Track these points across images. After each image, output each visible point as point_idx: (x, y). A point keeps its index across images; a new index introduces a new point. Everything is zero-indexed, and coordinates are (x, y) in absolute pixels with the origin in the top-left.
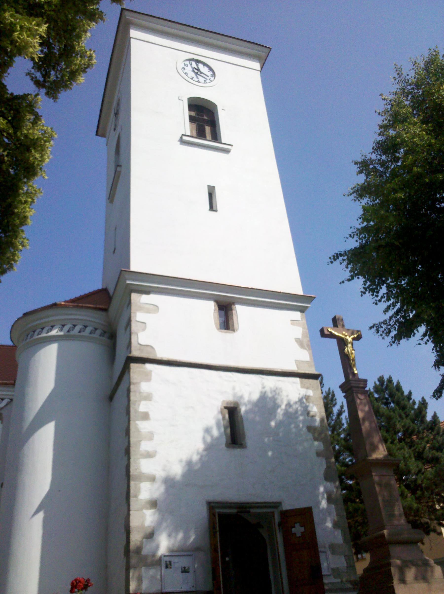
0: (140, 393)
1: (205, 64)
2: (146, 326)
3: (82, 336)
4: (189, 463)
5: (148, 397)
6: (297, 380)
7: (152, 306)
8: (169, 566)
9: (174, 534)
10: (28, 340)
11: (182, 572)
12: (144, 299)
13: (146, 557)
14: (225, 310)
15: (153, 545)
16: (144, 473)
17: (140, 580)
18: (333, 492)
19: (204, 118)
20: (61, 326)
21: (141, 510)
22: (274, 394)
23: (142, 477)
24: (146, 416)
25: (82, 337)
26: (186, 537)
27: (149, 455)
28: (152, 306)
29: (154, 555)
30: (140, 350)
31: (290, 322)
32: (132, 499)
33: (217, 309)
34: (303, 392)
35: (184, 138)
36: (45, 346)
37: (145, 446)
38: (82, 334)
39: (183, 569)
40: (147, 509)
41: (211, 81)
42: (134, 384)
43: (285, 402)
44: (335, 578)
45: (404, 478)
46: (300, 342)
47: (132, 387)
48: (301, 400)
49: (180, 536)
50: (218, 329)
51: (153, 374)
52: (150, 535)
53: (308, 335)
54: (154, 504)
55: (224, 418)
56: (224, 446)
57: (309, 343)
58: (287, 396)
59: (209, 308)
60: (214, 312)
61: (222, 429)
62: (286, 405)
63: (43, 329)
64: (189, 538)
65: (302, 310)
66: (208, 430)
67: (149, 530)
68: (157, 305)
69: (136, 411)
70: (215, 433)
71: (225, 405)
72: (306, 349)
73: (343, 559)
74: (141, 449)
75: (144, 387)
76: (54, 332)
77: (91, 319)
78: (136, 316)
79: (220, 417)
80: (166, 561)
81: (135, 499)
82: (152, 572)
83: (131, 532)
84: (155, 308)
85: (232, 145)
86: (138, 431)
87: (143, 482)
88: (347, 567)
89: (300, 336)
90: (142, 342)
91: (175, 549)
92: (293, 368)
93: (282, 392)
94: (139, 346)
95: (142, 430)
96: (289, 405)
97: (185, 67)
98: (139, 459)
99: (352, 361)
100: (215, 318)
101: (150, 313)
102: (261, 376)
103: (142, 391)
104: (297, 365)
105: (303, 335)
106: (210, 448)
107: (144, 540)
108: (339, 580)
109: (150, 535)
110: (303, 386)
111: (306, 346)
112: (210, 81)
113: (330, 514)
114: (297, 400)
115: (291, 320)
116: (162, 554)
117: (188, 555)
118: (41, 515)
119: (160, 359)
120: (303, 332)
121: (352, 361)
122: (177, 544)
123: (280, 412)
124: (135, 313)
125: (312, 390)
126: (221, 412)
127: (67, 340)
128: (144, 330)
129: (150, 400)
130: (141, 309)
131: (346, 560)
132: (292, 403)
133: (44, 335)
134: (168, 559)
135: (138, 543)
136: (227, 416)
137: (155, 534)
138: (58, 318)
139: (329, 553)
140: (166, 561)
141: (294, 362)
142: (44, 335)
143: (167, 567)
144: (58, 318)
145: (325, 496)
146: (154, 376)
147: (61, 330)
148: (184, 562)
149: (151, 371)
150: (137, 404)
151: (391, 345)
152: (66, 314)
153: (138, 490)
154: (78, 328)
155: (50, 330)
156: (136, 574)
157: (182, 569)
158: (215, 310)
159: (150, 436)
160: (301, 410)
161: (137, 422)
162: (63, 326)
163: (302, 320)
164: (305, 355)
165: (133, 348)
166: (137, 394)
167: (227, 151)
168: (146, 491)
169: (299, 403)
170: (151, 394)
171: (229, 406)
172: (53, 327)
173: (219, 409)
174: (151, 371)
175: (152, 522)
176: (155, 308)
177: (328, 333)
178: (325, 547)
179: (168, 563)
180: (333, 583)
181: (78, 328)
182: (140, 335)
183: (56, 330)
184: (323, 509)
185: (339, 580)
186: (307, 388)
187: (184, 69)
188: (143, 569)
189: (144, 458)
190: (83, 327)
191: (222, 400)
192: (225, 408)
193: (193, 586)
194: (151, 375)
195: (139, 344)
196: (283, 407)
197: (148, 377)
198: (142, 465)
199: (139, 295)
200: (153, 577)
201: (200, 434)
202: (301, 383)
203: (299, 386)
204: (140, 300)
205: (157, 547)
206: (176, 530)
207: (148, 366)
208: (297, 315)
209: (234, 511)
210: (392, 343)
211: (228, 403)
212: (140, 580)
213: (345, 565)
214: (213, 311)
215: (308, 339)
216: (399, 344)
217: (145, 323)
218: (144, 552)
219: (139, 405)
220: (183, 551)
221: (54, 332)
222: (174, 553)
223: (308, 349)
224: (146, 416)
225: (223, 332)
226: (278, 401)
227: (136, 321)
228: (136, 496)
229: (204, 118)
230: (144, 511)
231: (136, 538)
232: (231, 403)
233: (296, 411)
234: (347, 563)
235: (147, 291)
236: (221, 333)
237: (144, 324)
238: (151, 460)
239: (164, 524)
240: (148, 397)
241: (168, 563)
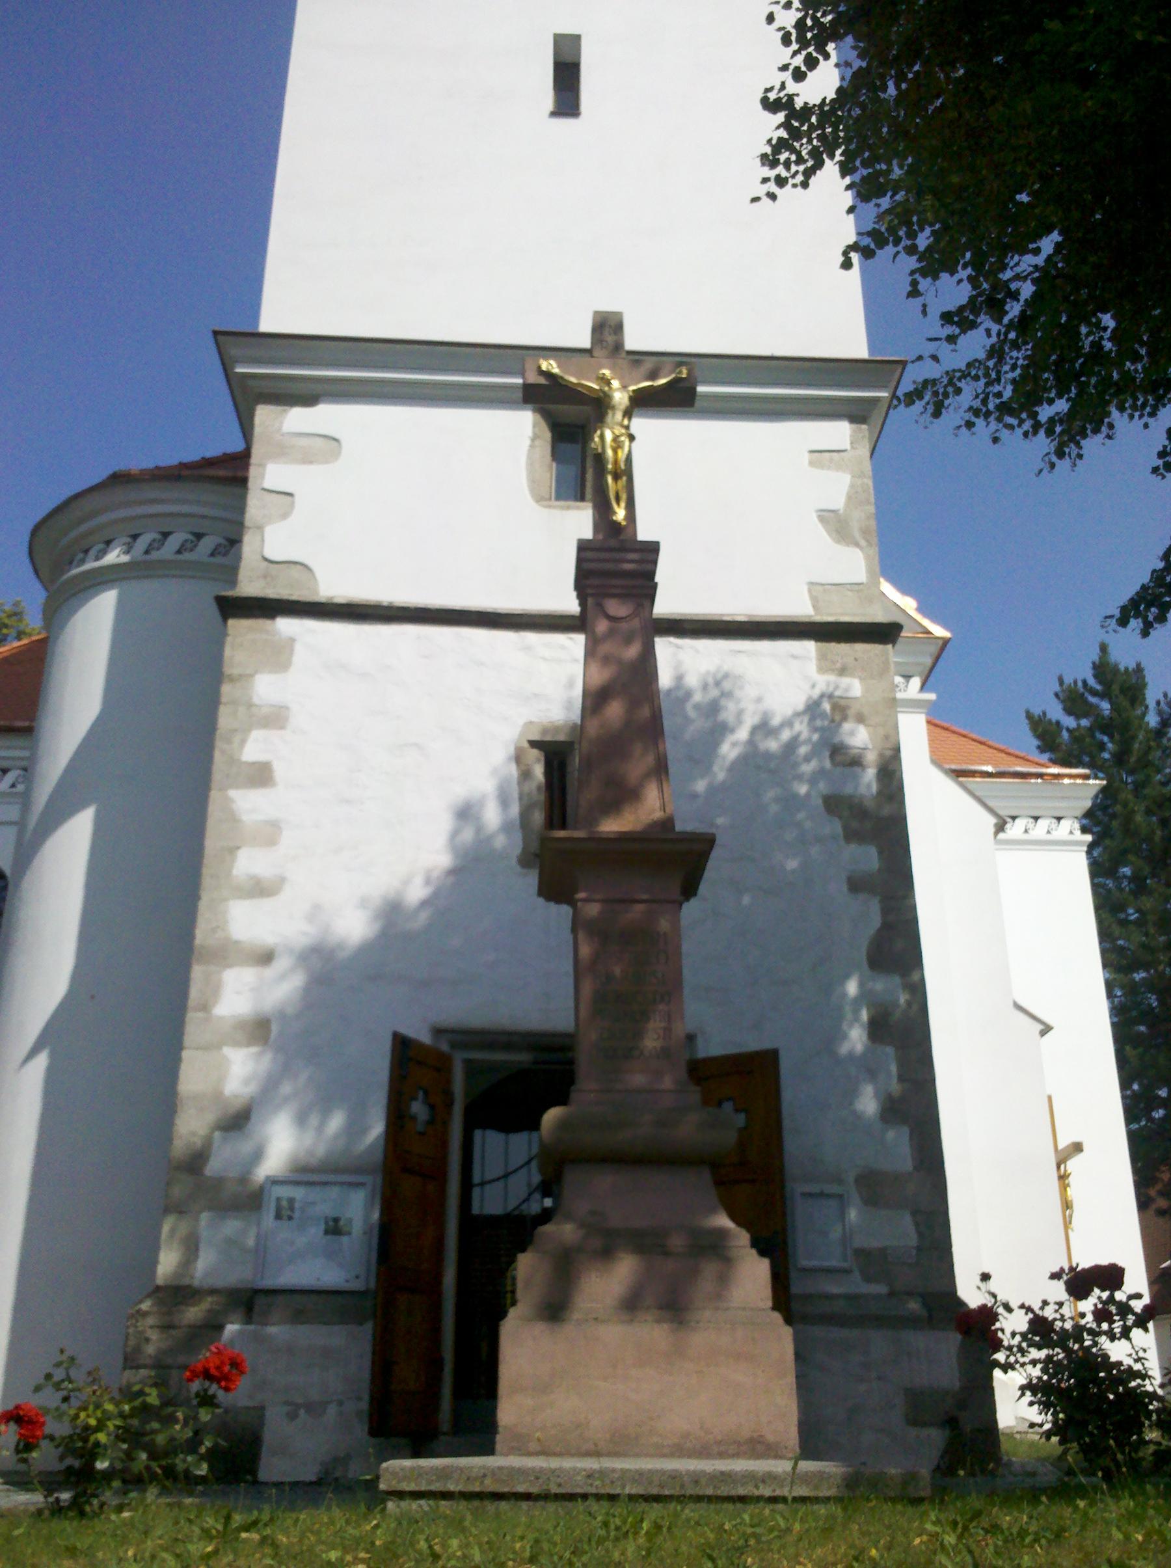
0: (250, 705)
2: (292, 505)
3: (186, 562)
4: (391, 913)
6: (809, 647)
7: (319, 442)
8: (285, 1213)
9: (314, 1120)
11: (326, 1232)
12: (297, 419)
13: (219, 1182)
15: (245, 1147)
16: (237, 942)
17: (191, 1248)
18: (895, 1004)
20: (129, 540)
21: (219, 1047)
22: (714, 693)
23: (228, 953)
24: (261, 775)
25: (163, 563)
26: (354, 1128)
27: (261, 889)
28: (319, 441)
29: (244, 1179)
30: (265, 577)
31: (807, 456)
32: (193, 1018)
33: (548, 435)
34: (824, 682)
36: (87, 600)
37: (249, 863)
38: (187, 556)
39: (331, 1223)
40: (237, 1044)
42: (232, 679)
43: (750, 721)
44: (868, 1279)
46: (836, 525)
47: (226, 689)
48: (812, 709)
49: (336, 1122)
50: (539, 499)
51: (298, 647)
52: (238, 1121)
53: (872, 500)
54: (258, 1030)
55: (525, 775)
56: (514, 861)
57: (873, 523)
58: (759, 700)
59: (513, 436)
60: (532, 446)
61: (515, 810)
62: (755, 730)
63: (86, 551)
64: (365, 1131)
65: (856, 413)
66: (466, 813)
67: (238, 1104)
68: (337, 437)
69: (233, 761)
70: (492, 816)
71: (536, 737)
72: (857, 545)
73: (907, 1221)
74: (235, 872)
75: (266, 688)
76: (114, 556)
77: (206, 511)
78: (263, 476)
79: (513, 770)
80: (278, 1199)
81: (200, 1015)
82: (232, 1226)
83: (179, 1109)
86: (233, 818)
87: (230, 966)
88: (919, 1249)
89: (838, 502)
90: (274, 551)
91: (314, 1161)
92: (801, 608)
93: (741, 688)
94: (265, 564)
95: (244, 818)
96: (764, 728)
98: (226, 900)
99: (610, 479)
101: (311, 462)
103: (256, 700)
105: (849, 498)
106: (470, 864)
107: (217, 1134)
108: (881, 1289)
109: (238, 1121)
111: (857, 535)
113: (872, 1075)
114: (801, 707)
115: (812, 452)
116: (268, 1178)
117: (342, 1184)
119: (323, 600)
120: (852, 486)
121: (610, 479)
122: (321, 1151)
123: (730, 750)
124: (262, 466)
125: (860, 679)
126: (518, 758)
127: (147, 577)
128: (285, 516)
129: (282, 728)
130: (282, 451)
131: (917, 1224)
132: (776, 721)
134: (284, 1192)
135: (198, 1142)
136: (539, 771)
137: (254, 1118)
138: (112, 516)
140: (278, 1199)
141: (805, 588)
143: (278, 1216)
144: (112, 516)
145: (864, 1015)
146: (300, 655)
147: (127, 552)
148: (325, 1202)
149: (292, 640)
150: (237, 739)
151: (1053, 466)
152: (141, 503)
153: (216, 990)
154: (207, 544)
155: (104, 552)
156: (183, 1228)
157: (326, 1223)
158: (534, 438)
159: (270, 834)
160: (809, 740)
161: (232, 793)
162: (135, 537)
163: (852, 448)
164: (852, 564)
165: (244, 574)
166: (242, 710)
168: (238, 993)
169: (806, 719)
170: (287, 708)
171: (548, 738)
172: (108, 543)
173: (512, 750)
174: (292, 640)
175: (247, 1082)
177: (542, 381)
178: (840, 1182)
179: (284, 1203)
180: (851, 1298)
181: (174, 542)
182: (270, 532)
183: (116, 552)
184: (851, 1056)
185: (881, 1289)
186: (843, 671)
188: (205, 1217)
189: (240, 898)
190: (191, 537)
191: (521, 722)
192: (533, 744)
193: (357, 1277)
194: (292, 651)
195: (266, 559)
196: (743, 734)
197: (280, 657)
198: (243, 921)
199: (279, 408)
200: (230, 1242)
201: (444, 823)
202: (822, 657)
203: (812, 667)
204: (282, 423)
205: (258, 1155)
206: (325, 1104)
207: (285, 625)
208: (839, 433)
209: (522, 1058)
210: (1054, 459)
211: (545, 731)
212: (191, 1248)
213: (912, 1240)
214: (528, 442)
215: (872, 509)
216: (1080, 456)
217: (290, 495)
218: (214, 1167)
219: (243, 742)
220: (337, 1170)
221: (114, 556)
222: (305, 1174)
223: (863, 543)
225: (555, 507)
226: (728, 714)
227: (264, 489)
228: (205, 1008)
230: (227, 1051)
231: (191, 1126)
232: (556, 729)
233: (791, 746)
234: (920, 1234)
236: (547, 510)
237: (289, 498)
238: (266, 903)
239: (286, 1088)
240: (276, 719)
241: (284, 1203)
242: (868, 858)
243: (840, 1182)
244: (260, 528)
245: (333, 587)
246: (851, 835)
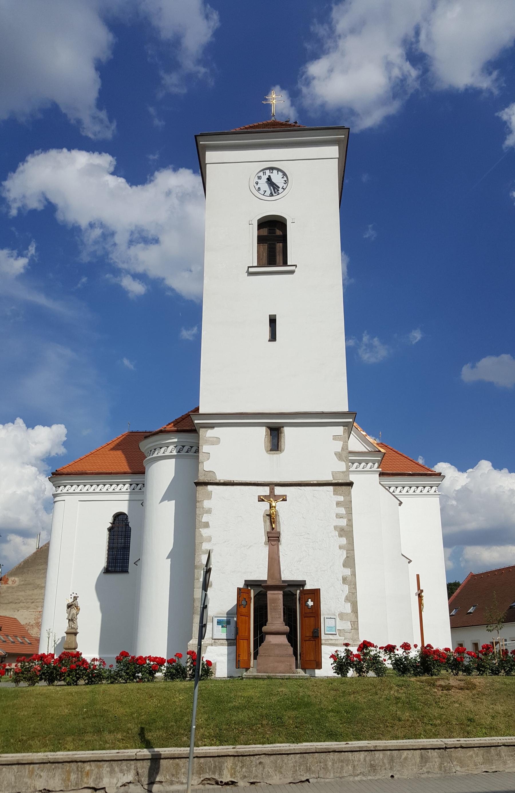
1: (124, 683)
5: (209, 511)
6: (331, 488)
10: (154, 456)
14: (275, 433)
19: (273, 237)
24: (207, 525)
35: (251, 270)
37: (205, 518)
41: (284, 189)
44: (340, 636)
45: (126, 362)
69: (200, 521)
72: (344, 461)
84: (216, 441)
85: (296, 266)
92: (329, 478)
97: (259, 181)
100: (265, 442)
102: (299, 487)
104: (333, 475)
110: (335, 493)
112: (283, 190)
118: (170, 506)
120: (343, 445)
128: (208, 459)
133: (155, 455)
139: (338, 619)
142: (155, 455)
166: (201, 509)
167: (292, 272)
176: (216, 441)
178: (335, 615)
187: (257, 183)
197: (209, 496)
202: (334, 491)
207: (210, 487)
224: (207, 525)
229: (273, 237)
235: (212, 426)
236: (269, 455)
242: (344, 541)
243: (335, 615)
244: (203, 462)
245: (221, 477)
246: (340, 536)
